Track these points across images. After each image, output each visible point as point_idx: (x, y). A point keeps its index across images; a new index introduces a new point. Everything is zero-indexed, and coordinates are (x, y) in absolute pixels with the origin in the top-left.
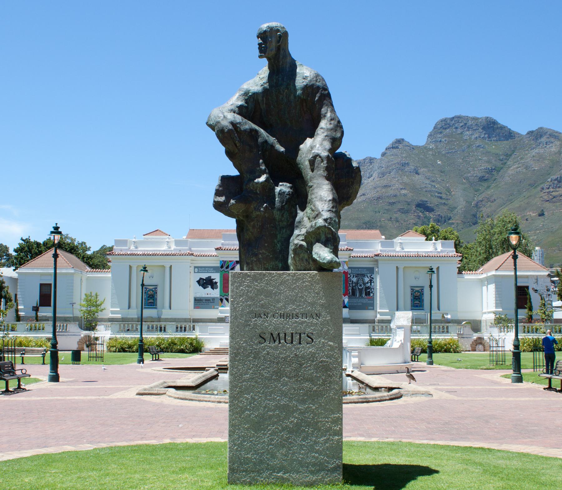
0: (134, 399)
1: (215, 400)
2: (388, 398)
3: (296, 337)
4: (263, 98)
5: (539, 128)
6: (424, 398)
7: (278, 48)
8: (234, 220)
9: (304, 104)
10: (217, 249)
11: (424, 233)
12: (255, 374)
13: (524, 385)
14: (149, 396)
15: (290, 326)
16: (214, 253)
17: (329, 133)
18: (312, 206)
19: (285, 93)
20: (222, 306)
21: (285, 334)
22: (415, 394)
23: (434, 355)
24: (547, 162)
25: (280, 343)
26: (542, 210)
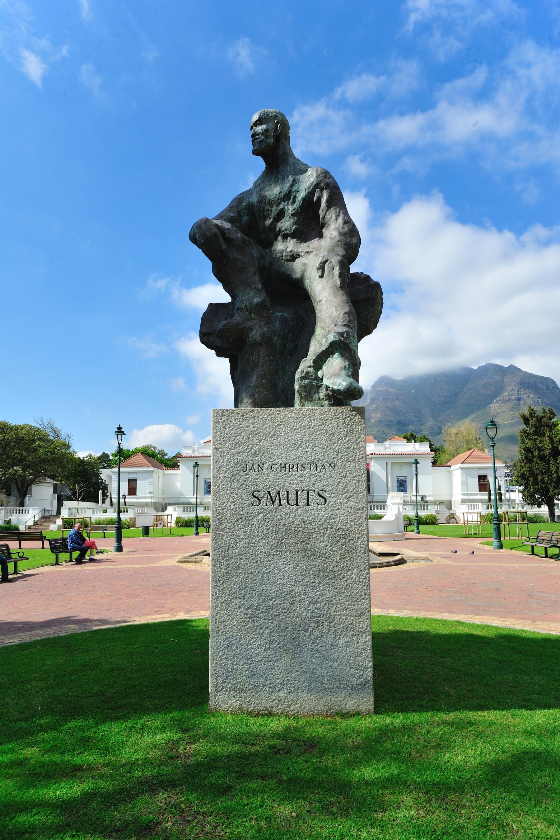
0: (174, 566)
2: (393, 564)
3: (297, 498)
6: (423, 564)
11: (405, 438)
12: (247, 547)
13: (505, 551)
14: (188, 563)
15: (293, 481)
17: (342, 237)
21: (288, 492)
22: (416, 559)
23: (420, 526)
24: (492, 388)
25: (280, 505)
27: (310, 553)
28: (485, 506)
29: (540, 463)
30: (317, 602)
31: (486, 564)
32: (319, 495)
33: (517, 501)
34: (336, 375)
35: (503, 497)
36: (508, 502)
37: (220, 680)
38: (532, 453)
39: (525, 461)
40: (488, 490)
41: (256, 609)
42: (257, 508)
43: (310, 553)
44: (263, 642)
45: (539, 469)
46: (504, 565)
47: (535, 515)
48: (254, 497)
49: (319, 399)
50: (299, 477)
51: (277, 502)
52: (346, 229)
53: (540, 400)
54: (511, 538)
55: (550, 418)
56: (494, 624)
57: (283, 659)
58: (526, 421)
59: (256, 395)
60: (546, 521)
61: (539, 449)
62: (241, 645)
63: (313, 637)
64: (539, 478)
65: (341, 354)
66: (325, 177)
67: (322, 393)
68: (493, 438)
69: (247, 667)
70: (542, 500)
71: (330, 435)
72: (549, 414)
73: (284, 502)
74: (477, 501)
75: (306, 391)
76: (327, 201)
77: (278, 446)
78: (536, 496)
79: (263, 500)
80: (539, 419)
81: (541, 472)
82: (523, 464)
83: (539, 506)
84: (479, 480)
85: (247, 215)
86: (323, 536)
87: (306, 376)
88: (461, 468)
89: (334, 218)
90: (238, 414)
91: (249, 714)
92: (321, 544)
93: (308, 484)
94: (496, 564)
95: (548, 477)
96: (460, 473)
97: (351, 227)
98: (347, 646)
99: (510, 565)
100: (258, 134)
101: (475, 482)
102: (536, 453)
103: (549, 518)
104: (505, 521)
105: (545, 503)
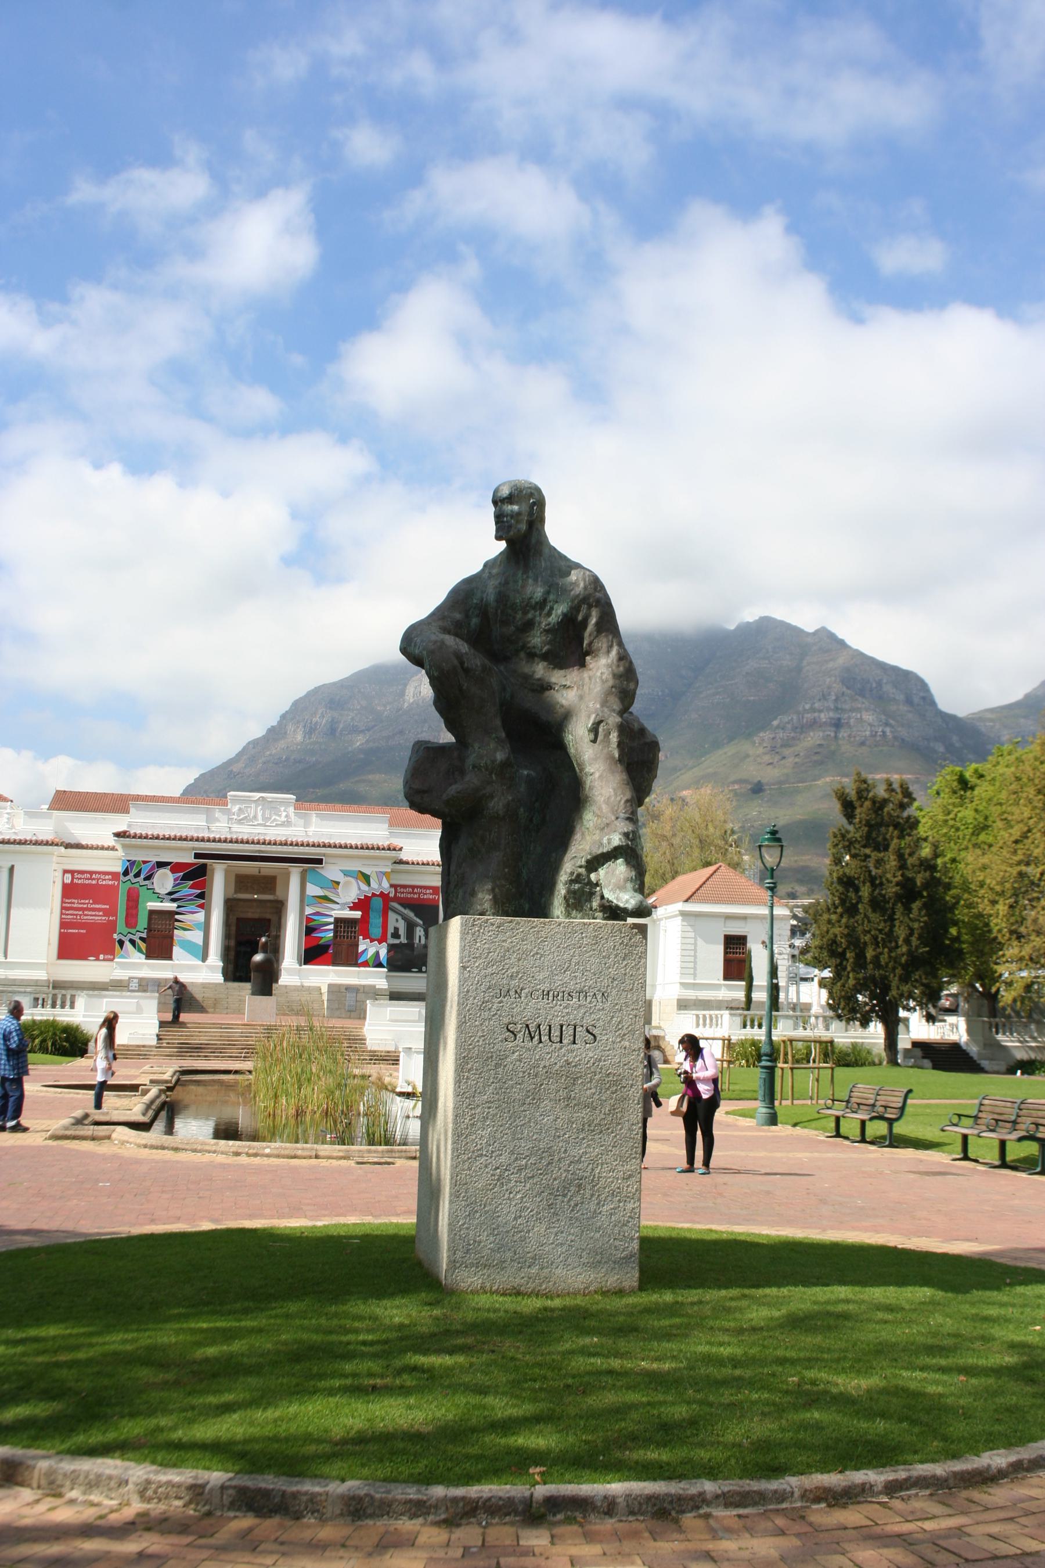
0: (39, 1147)
1: (227, 1149)
10: (118, 835)
12: (497, 1093)
13: (782, 1130)
15: (558, 1013)
16: (111, 841)
20: (123, 957)
25: (541, 1042)
27: (574, 1102)
28: (738, 1020)
29: (873, 916)
30: (579, 1161)
31: (743, 1154)
32: (588, 1031)
33: (815, 1009)
34: (622, 888)
35: (782, 995)
36: (794, 1009)
37: (459, 1254)
38: (857, 890)
39: (840, 910)
40: (746, 975)
41: (506, 1170)
42: (511, 1044)
43: (574, 1102)
44: (513, 1209)
45: (869, 932)
46: (778, 1155)
47: (854, 1045)
48: (509, 1030)
49: (591, 909)
50: (565, 1007)
51: (537, 1038)
52: (621, 669)
53: (888, 730)
54: (795, 1102)
55: (902, 806)
56: (764, 1232)
57: (536, 1229)
58: (848, 807)
59: (497, 890)
60: (877, 1061)
61: (872, 880)
62: (486, 1212)
63: (572, 1203)
64: (870, 953)
65: (626, 860)
66: (595, 589)
67: (595, 904)
68: (772, 870)
69: (492, 1239)
70: (872, 1010)
71: (604, 957)
72: (900, 796)
73: (545, 1038)
74: (719, 1005)
75: (575, 899)
76: (597, 624)
77: (541, 968)
78: (860, 998)
79: (520, 1035)
80: (878, 805)
81: (875, 938)
82: (834, 917)
83: (865, 1023)
84: (726, 948)
85: (478, 616)
86: (591, 1082)
87: (578, 879)
88: (684, 914)
89: (605, 646)
90: (493, 925)
91: (497, 1292)
93: (576, 1016)
94: (763, 1154)
95: (890, 951)
96: (679, 928)
97: (627, 665)
98: (611, 1214)
99: (791, 1155)
100: (507, 516)
101: (715, 955)
102: (865, 891)
103: (884, 1054)
104: (786, 1062)
105: (878, 1016)
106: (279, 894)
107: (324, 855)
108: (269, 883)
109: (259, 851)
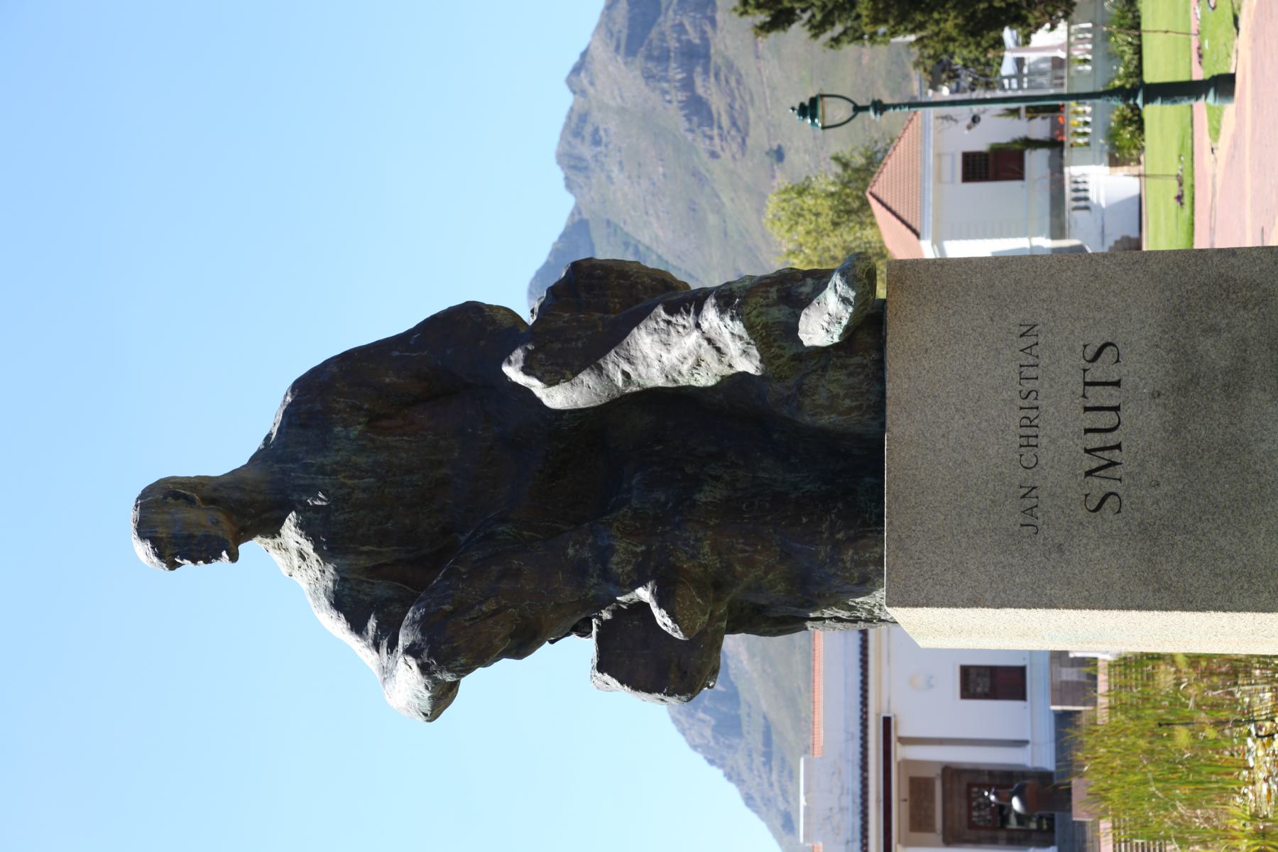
3: (1103, 419)
4: (362, 553)
5: (559, 162)
7: (211, 501)
8: (726, 637)
9: (385, 423)
18: (685, 368)
19: (350, 482)
21: (1087, 431)
26: (767, 153)
51: (1106, 454)
73: (1111, 439)
92: (1215, 353)
106: (935, 773)
107: (878, 715)
108: (919, 788)
109: (878, 801)
